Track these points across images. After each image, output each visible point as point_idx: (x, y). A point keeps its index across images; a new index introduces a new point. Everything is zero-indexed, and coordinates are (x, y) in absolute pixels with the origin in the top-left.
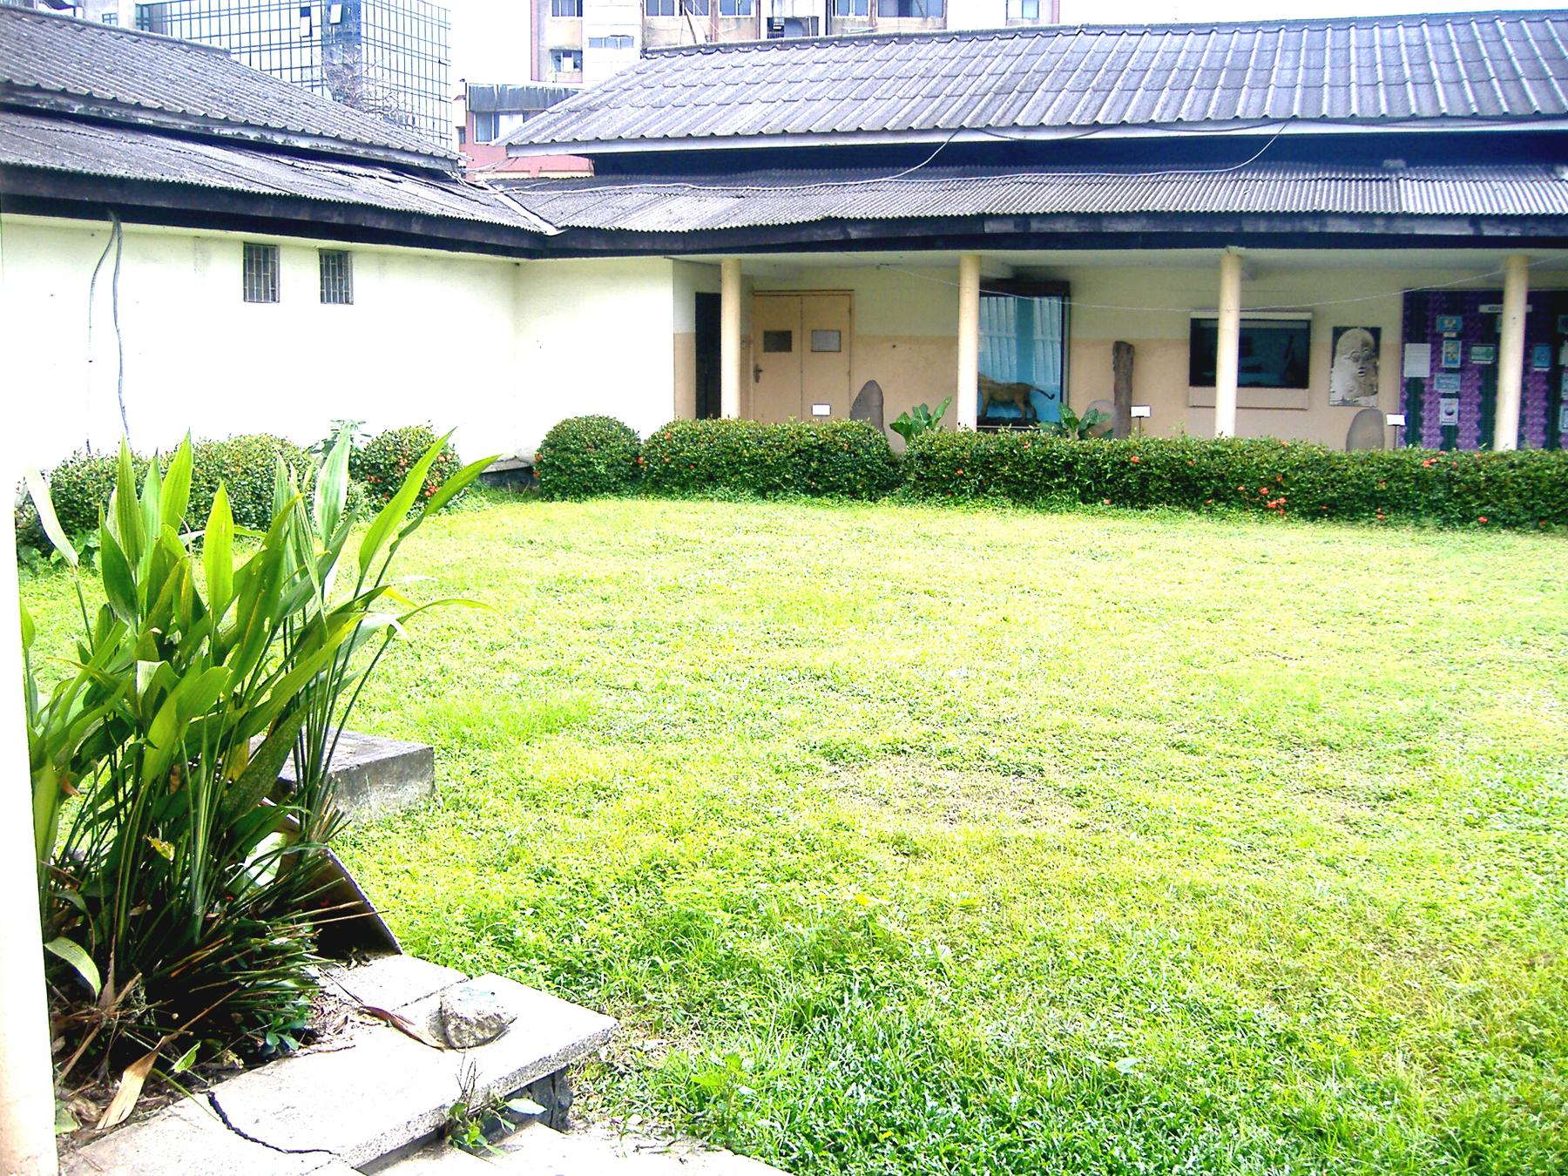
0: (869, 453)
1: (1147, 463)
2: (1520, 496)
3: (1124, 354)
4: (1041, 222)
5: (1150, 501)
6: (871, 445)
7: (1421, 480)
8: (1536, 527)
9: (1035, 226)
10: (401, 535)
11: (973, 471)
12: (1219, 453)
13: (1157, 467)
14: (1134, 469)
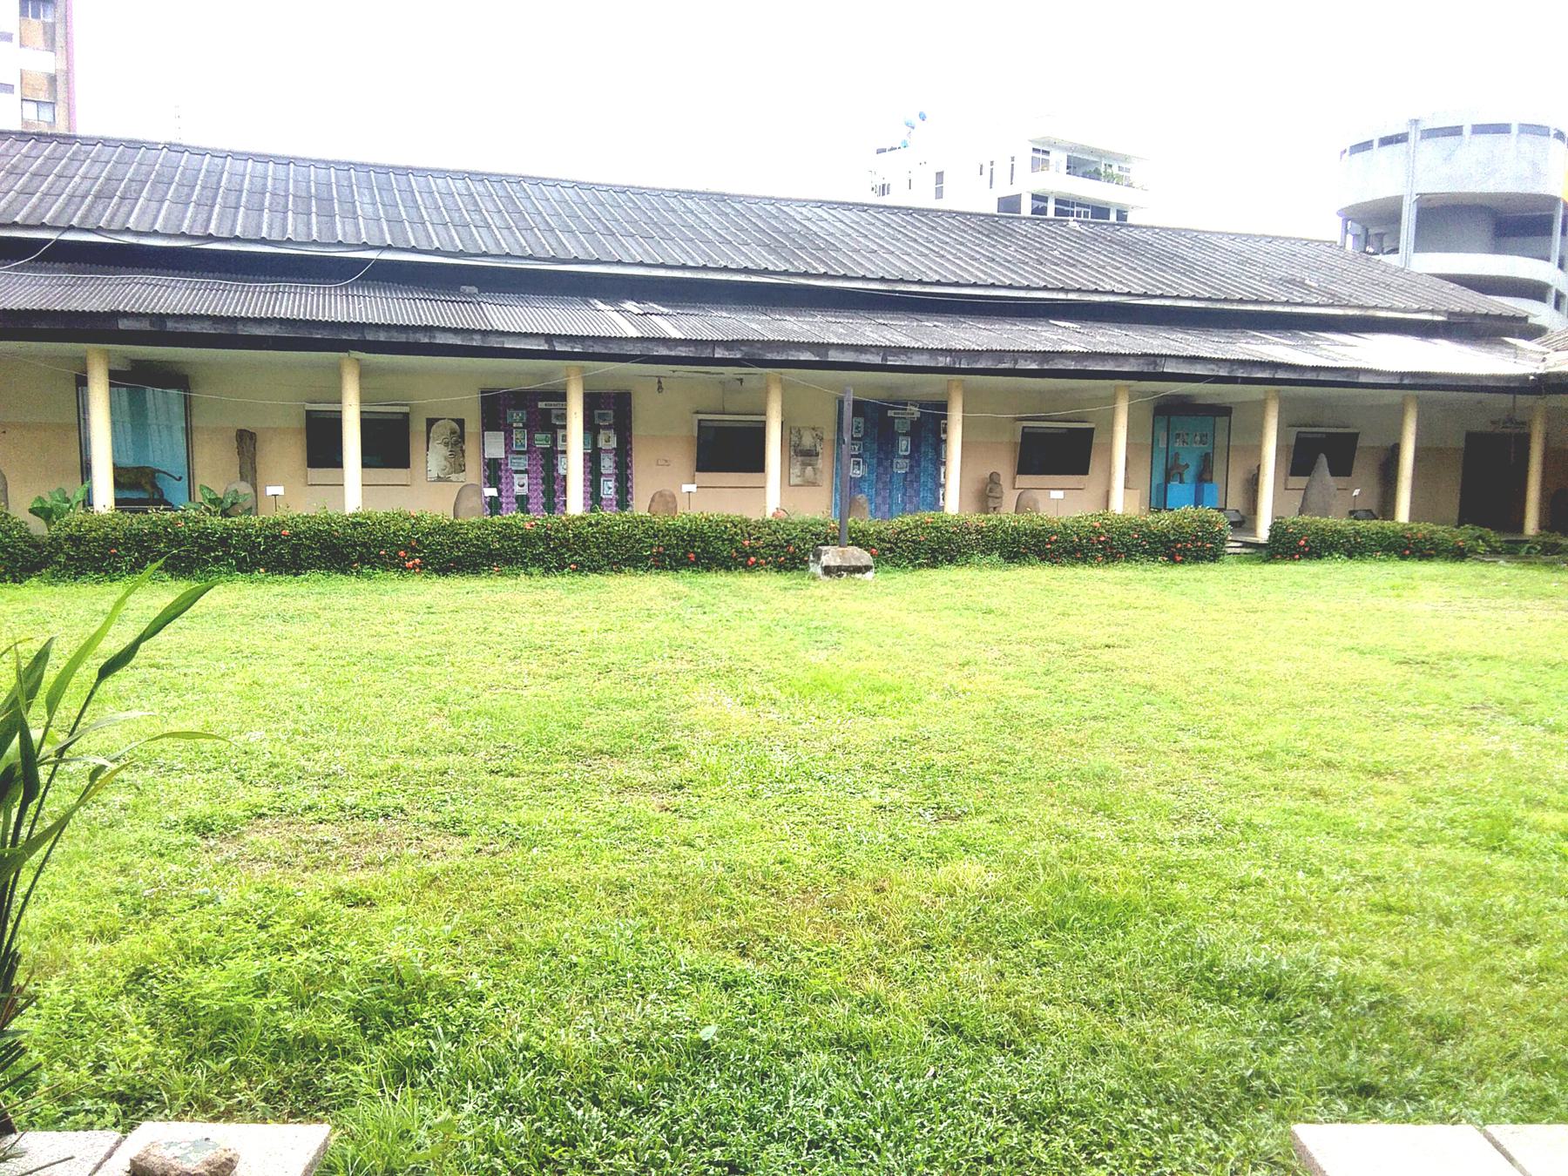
0: (10, 537)
1: (296, 535)
2: (598, 548)
3: (246, 442)
4: (176, 322)
5: (302, 567)
6: (10, 529)
7: (527, 540)
8: (612, 570)
9: (170, 325)
10: (106, 671)
11: (128, 550)
12: (360, 524)
13: (307, 538)
14: (285, 541)
